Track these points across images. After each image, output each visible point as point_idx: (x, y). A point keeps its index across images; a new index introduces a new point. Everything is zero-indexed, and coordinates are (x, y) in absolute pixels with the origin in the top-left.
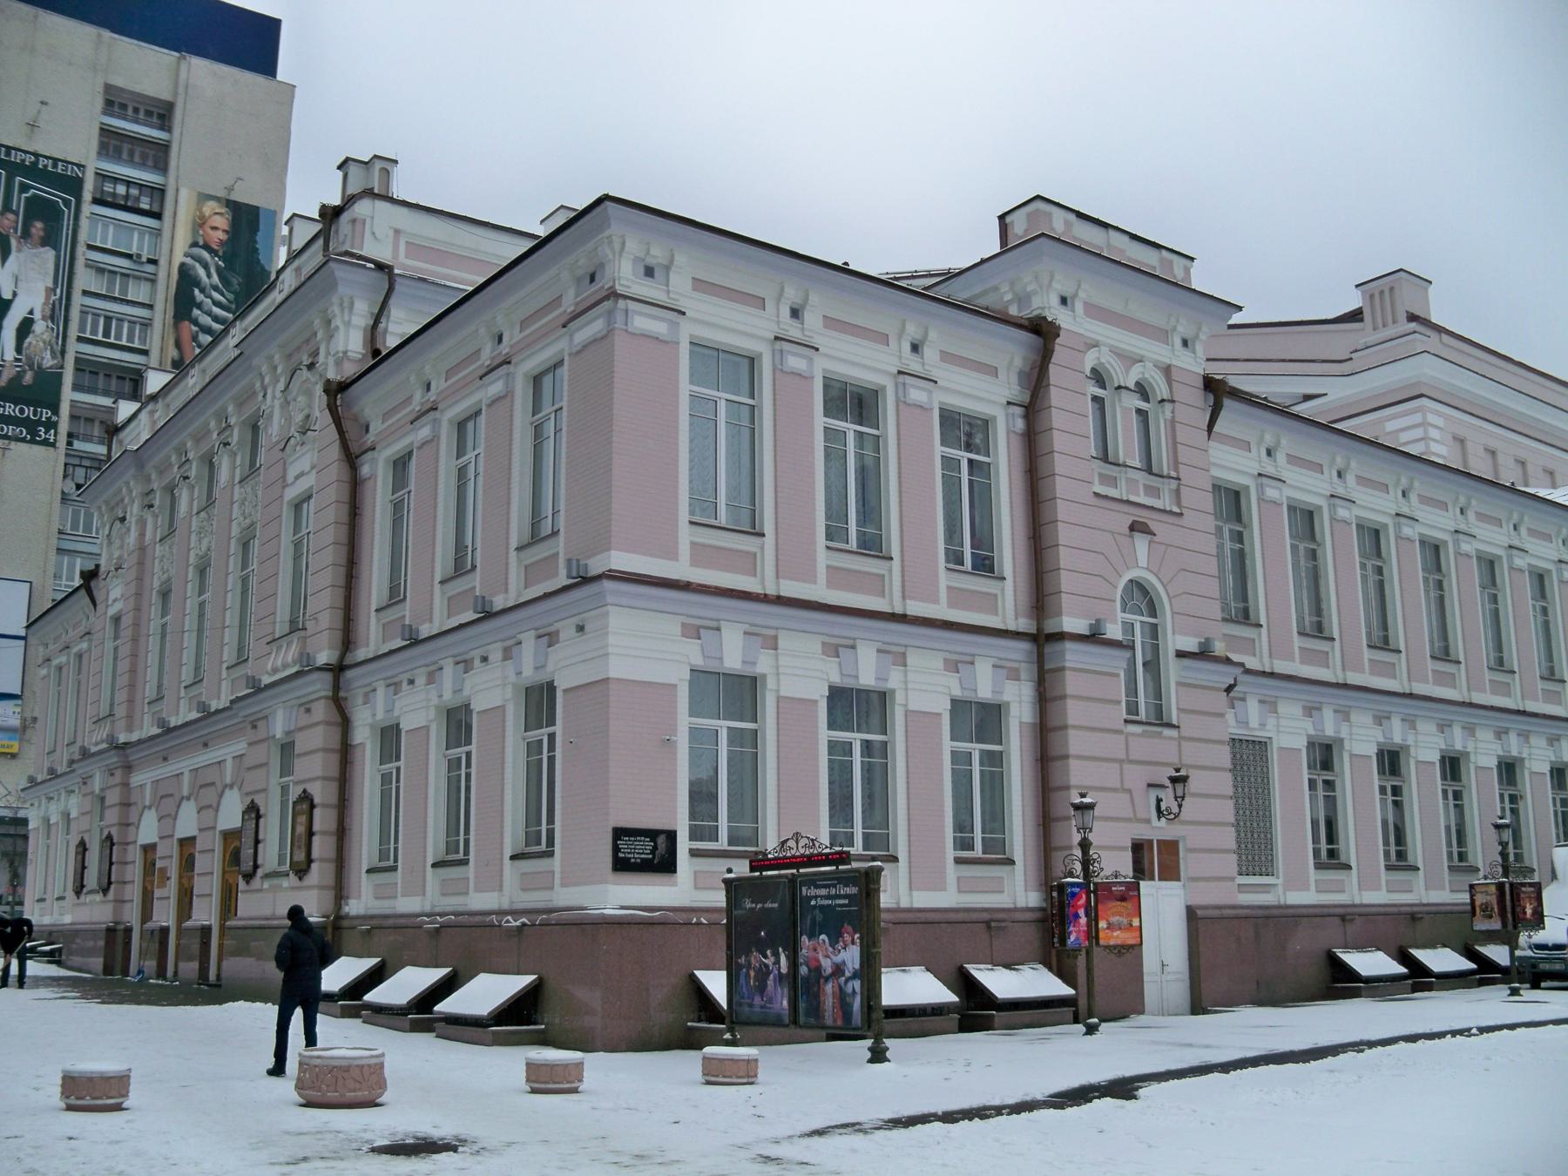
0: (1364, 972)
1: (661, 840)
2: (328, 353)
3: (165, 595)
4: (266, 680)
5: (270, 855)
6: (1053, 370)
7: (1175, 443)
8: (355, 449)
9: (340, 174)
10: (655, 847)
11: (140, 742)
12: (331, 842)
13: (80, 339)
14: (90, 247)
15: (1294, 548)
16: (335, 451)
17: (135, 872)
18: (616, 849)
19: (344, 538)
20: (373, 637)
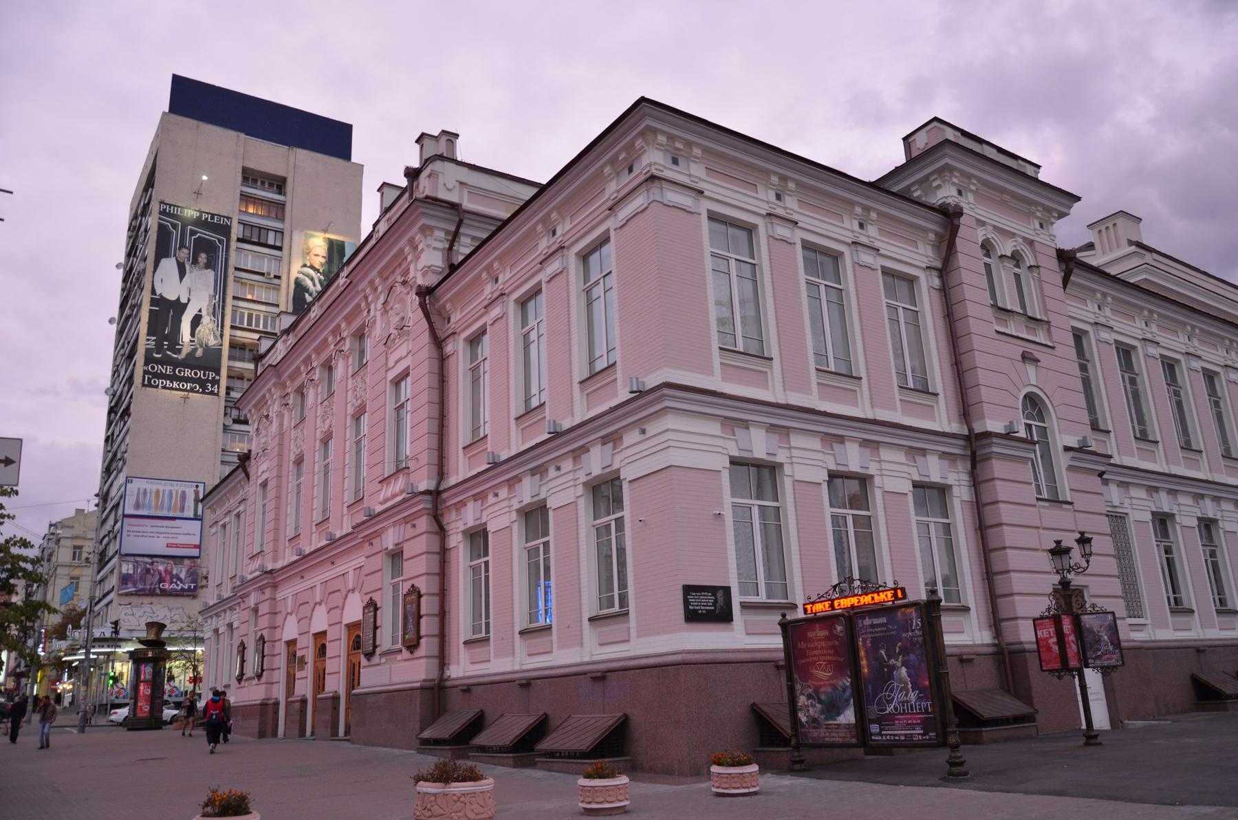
0: (1228, 692)
1: (720, 594)
2: (416, 270)
3: (299, 462)
4: (379, 508)
5: (386, 638)
6: (958, 240)
7: (1043, 296)
8: (441, 335)
9: (418, 146)
10: (716, 601)
11: (283, 568)
12: (435, 621)
13: (232, 327)
14: (236, 269)
15: (1123, 377)
16: (426, 337)
17: (281, 662)
18: (686, 603)
19: (436, 399)
20: (461, 468)
